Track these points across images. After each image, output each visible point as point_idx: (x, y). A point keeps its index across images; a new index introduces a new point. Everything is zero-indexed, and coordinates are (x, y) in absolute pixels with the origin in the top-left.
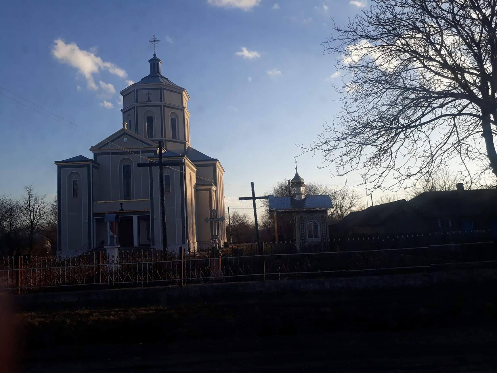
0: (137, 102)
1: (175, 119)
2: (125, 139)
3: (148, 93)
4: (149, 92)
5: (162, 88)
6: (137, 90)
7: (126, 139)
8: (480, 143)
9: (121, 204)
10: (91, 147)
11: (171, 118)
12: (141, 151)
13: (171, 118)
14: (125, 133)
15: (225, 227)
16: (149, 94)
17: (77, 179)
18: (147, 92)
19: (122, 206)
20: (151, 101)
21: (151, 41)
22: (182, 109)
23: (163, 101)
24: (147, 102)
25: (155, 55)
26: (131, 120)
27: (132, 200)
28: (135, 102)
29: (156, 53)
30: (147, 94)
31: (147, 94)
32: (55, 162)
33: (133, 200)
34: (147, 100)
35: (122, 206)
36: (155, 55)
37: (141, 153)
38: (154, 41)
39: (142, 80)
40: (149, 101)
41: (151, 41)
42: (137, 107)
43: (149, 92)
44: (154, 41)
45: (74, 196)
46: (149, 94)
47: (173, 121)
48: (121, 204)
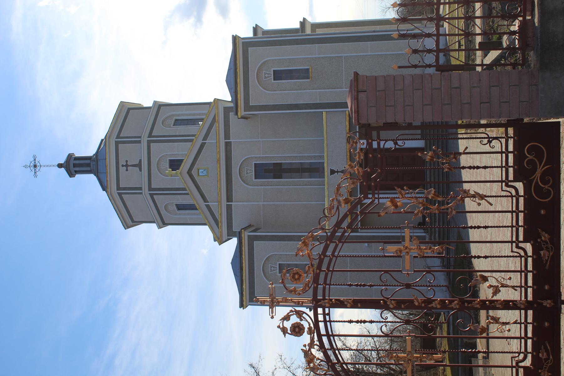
0: (140, 189)
1: (176, 120)
2: (200, 174)
3: (125, 168)
4: (123, 166)
5: (117, 140)
6: (119, 188)
7: (200, 171)
8: (426, 56)
9: (332, 172)
10: (215, 241)
11: (174, 125)
12: (225, 139)
13: (174, 125)
14: (188, 173)
15: (436, 72)
16: (127, 166)
17: (278, 263)
18: (122, 170)
19: (338, 172)
20: (140, 161)
21: (35, 160)
22: (159, 107)
23: (140, 139)
24: (141, 170)
25: (60, 166)
26: (177, 205)
27: (326, 161)
28: (141, 193)
29: (57, 164)
30: (127, 170)
31: (127, 170)
32: (240, 307)
33: (325, 158)
34: (137, 169)
35: (338, 172)
36: (60, 166)
37: (230, 139)
38: (35, 166)
39: (104, 190)
40: (139, 165)
41: (35, 160)
42: (150, 189)
43: (123, 166)
44: (35, 166)
45: (308, 78)
46: (127, 166)
47: (178, 122)
48: (332, 172)
